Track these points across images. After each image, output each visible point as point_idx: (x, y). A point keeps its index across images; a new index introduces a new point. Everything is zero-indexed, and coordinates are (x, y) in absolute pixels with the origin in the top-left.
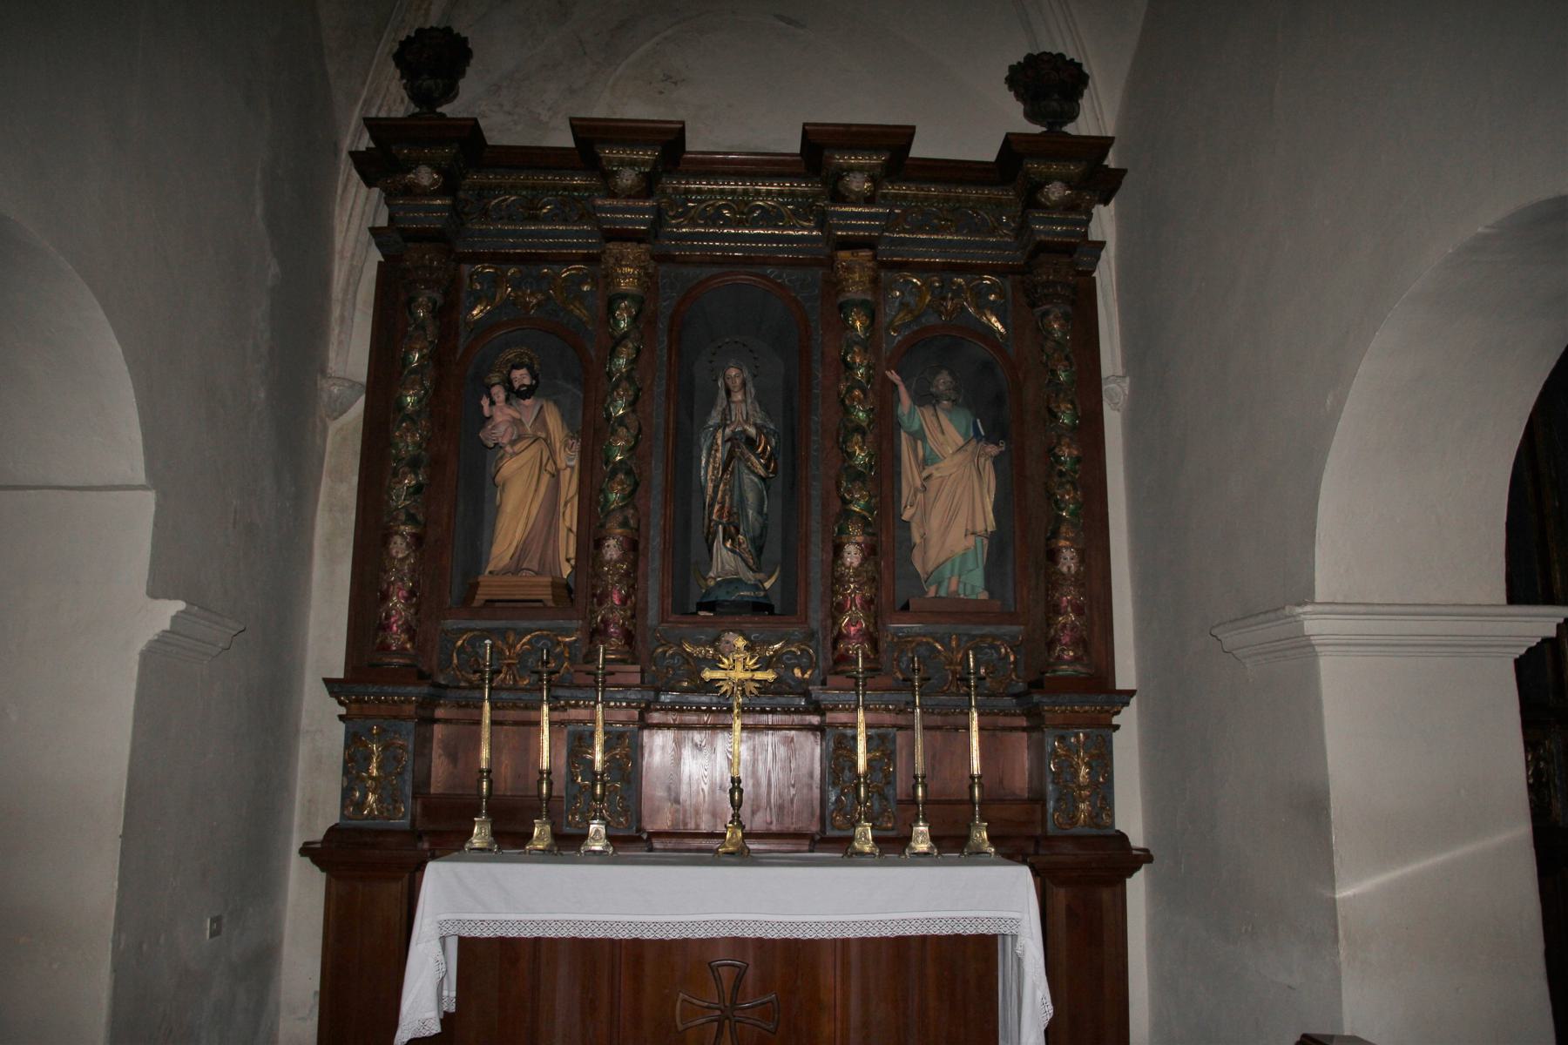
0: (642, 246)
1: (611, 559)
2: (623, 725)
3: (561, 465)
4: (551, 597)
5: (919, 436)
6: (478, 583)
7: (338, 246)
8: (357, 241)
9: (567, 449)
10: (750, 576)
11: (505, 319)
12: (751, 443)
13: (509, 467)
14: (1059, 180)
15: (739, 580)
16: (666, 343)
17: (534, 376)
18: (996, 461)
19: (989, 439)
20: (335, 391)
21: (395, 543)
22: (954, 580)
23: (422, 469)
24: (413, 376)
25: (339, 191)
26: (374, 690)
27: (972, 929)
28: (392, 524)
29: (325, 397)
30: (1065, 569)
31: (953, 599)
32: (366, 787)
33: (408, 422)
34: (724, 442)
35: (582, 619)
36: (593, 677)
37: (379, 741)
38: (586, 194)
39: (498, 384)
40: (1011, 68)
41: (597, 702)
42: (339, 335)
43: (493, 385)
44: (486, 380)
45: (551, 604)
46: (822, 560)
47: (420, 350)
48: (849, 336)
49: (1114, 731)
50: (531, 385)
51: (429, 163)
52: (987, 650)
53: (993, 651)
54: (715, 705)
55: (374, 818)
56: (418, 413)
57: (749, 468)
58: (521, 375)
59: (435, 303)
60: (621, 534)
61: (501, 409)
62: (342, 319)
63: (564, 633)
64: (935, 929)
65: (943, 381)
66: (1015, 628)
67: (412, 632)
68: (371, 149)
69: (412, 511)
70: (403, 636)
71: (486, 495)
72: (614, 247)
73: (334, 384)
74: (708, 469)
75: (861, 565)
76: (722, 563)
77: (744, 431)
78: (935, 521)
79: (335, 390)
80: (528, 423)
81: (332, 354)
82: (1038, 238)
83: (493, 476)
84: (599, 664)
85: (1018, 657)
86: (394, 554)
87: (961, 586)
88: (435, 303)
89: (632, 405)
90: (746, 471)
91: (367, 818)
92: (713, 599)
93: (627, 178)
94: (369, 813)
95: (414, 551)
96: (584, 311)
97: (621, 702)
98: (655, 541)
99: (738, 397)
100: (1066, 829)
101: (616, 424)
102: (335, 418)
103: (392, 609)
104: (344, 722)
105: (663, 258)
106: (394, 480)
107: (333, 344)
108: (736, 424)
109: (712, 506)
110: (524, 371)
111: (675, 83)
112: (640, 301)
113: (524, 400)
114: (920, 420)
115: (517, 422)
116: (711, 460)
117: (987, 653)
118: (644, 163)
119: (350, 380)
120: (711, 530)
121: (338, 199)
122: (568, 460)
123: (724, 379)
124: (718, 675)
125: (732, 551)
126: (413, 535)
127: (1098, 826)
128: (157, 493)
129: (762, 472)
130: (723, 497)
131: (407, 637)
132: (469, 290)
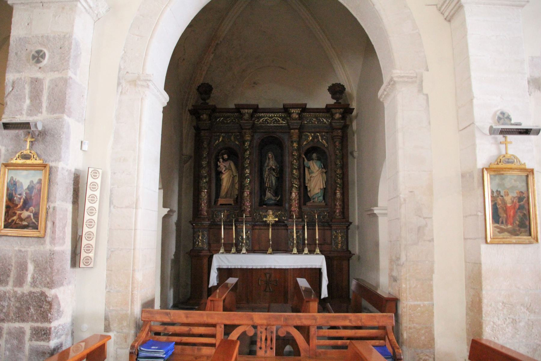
5: (309, 168)
10: (273, 198)
30: (337, 197)
34: (268, 170)
40: (329, 87)
56: (206, 167)
74: (266, 174)
93: (246, 116)
109: (266, 183)
111: (256, 84)
124: (267, 219)
129: (276, 176)
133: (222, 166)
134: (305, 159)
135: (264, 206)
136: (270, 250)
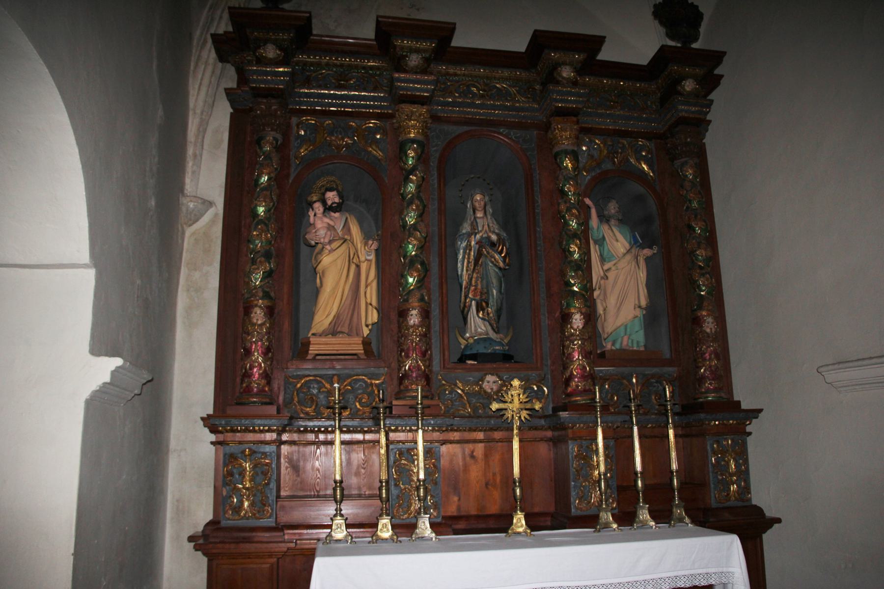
0: (425, 107)
1: (414, 324)
2: (431, 443)
3: (362, 258)
4: (363, 352)
5: (601, 242)
6: (310, 342)
7: (191, 104)
8: (205, 102)
9: (366, 248)
11: (323, 156)
12: (493, 245)
13: (326, 260)
14: (691, 78)
15: (490, 339)
16: (436, 175)
17: (341, 196)
18: (648, 260)
19: (642, 247)
20: (191, 206)
21: (256, 313)
22: (625, 339)
23: (273, 259)
24: (264, 192)
25: (192, 68)
26: (246, 422)
27: (705, 582)
28: (252, 299)
29: (184, 209)
30: (708, 330)
31: (622, 351)
32: (241, 495)
33: (262, 225)
35: (388, 368)
36: (414, 410)
37: (251, 460)
38: (378, 73)
39: (318, 201)
41: (418, 428)
42: (192, 167)
43: (315, 202)
44: (309, 199)
45: (363, 357)
46: (548, 325)
47: (268, 174)
48: (564, 174)
49: (748, 436)
50: (340, 202)
51: (276, 43)
52: (656, 384)
53: (659, 385)
54: (360, 426)
55: (248, 519)
57: (492, 262)
58: (333, 195)
59: (277, 140)
60: (419, 306)
61: (321, 219)
62: (195, 156)
63: (374, 377)
64: (681, 583)
65: (612, 208)
66: (671, 369)
67: (269, 379)
68: (230, 32)
69: (267, 290)
70: (263, 381)
71: (301, 280)
72: (407, 108)
73: (191, 201)
75: (583, 328)
76: (475, 326)
77: (489, 238)
78: (612, 301)
79: (191, 205)
80: (339, 229)
81: (188, 180)
82: (680, 115)
83: (315, 266)
84: (418, 400)
85: (674, 388)
86: (255, 321)
87: (630, 341)
88: (277, 140)
89: (421, 216)
90: (490, 264)
91: (242, 518)
92: (475, 352)
93: (414, 60)
94: (245, 515)
95: (269, 319)
96: (379, 152)
97: (406, 427)
98: (435, 312)
99: (479, 214)
100: (724, 503)
101: (412, 229)
102: (190, 225)
103: (254, 362)
104: (214, 446)
105: (435, 118)
106: (253, 267)
107: (188, 173)
108: (483, 232)
110: (335, 193)
111: (418, 10)
112: (421, 144)
113: (335, 213)
114: (603, 232)
115: (330, 228)
116: (467, 256)
117: (654, 386)
118: (424, 51)
119: (202, 199)
120: (467, 304)
121: (191, 72)
122: (367, 255)
123: (472, 201)
125: (482, 319)
126: (268, 307)
127: (743, 501)
128: (96, 270)
129: (501, 265)
130: (476, 282)
131: (266, 381)
132: (297, 135)
133: (319, 225)
134: (593, 212)
135: (469, 362)
136: (519, 521)
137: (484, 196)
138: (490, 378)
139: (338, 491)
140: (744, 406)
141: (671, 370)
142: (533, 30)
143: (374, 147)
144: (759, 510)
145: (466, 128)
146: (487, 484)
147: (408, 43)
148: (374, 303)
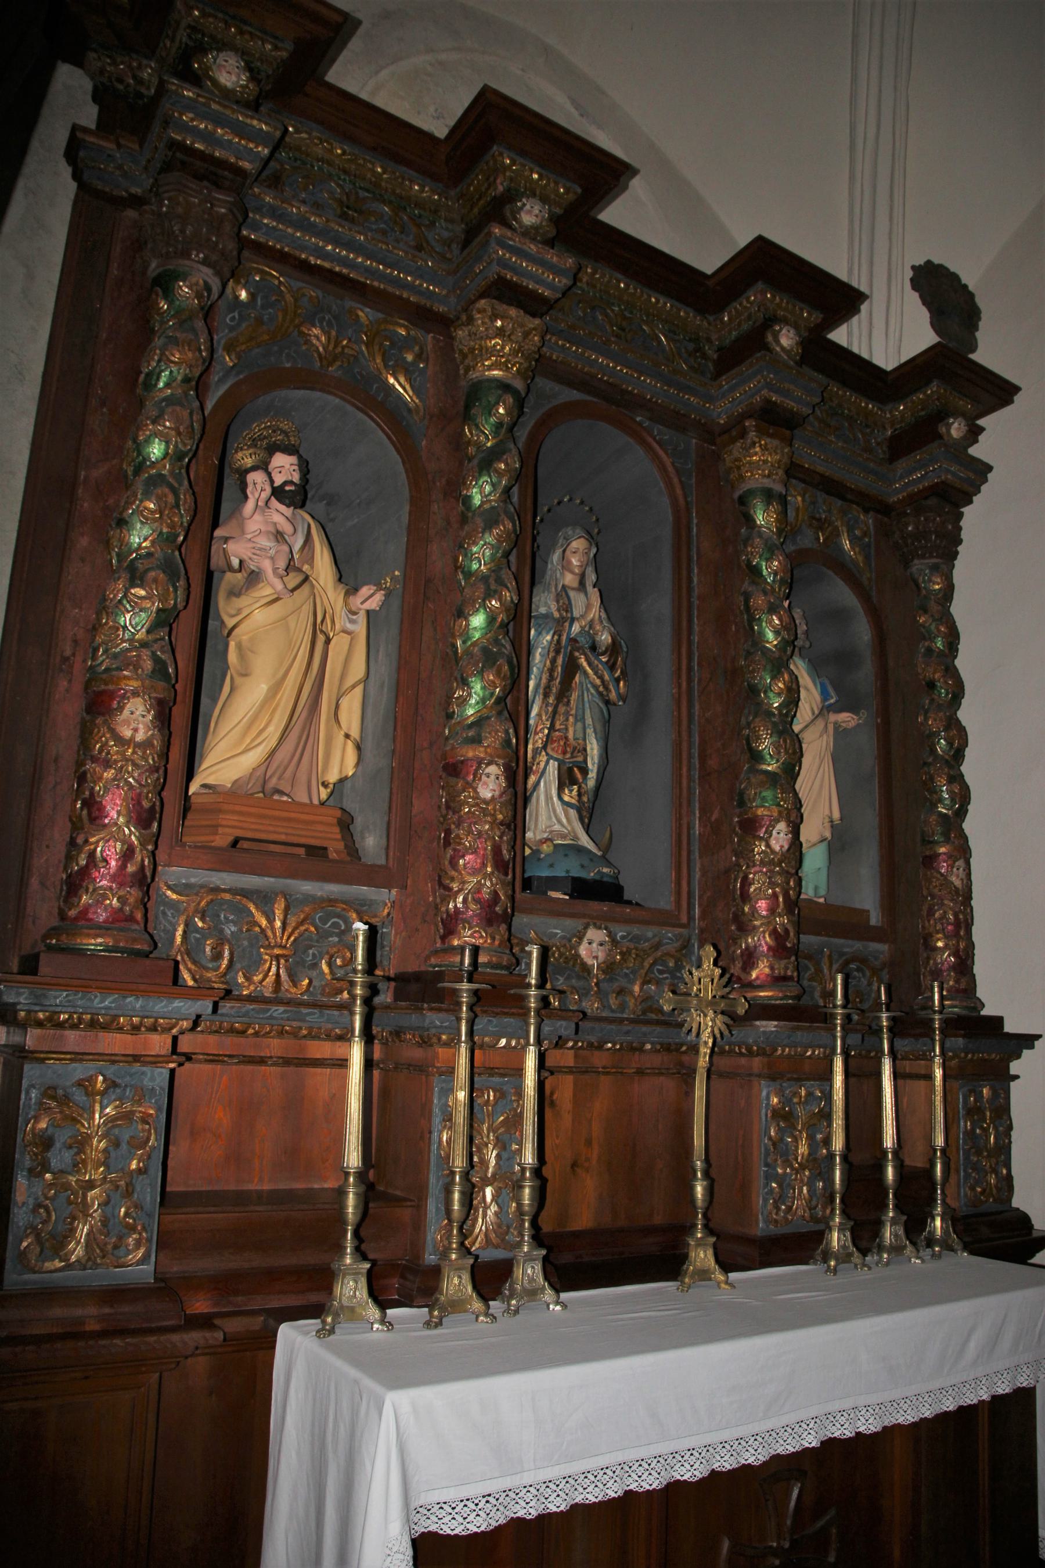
11: (288, 365)
110: (293, 459)
136: (702, 1256)
137: (591, 545)
138: (596, 935)
139: (351, 1196)
140: (1009, 1028)
141: (882, 948)
142: (756, 235)
143: (402, 380)
144: (1024, 1221)
145: (575, 395)
146: (574, 1165)
147: (422, 191)
148: (355, 733)
